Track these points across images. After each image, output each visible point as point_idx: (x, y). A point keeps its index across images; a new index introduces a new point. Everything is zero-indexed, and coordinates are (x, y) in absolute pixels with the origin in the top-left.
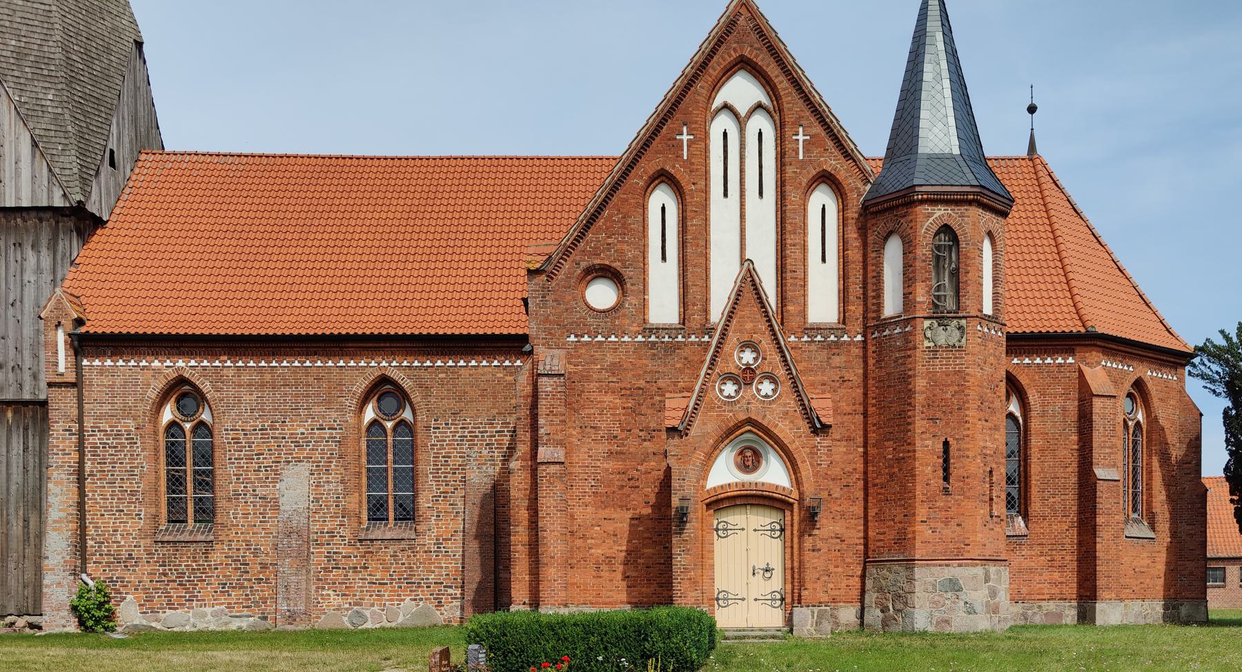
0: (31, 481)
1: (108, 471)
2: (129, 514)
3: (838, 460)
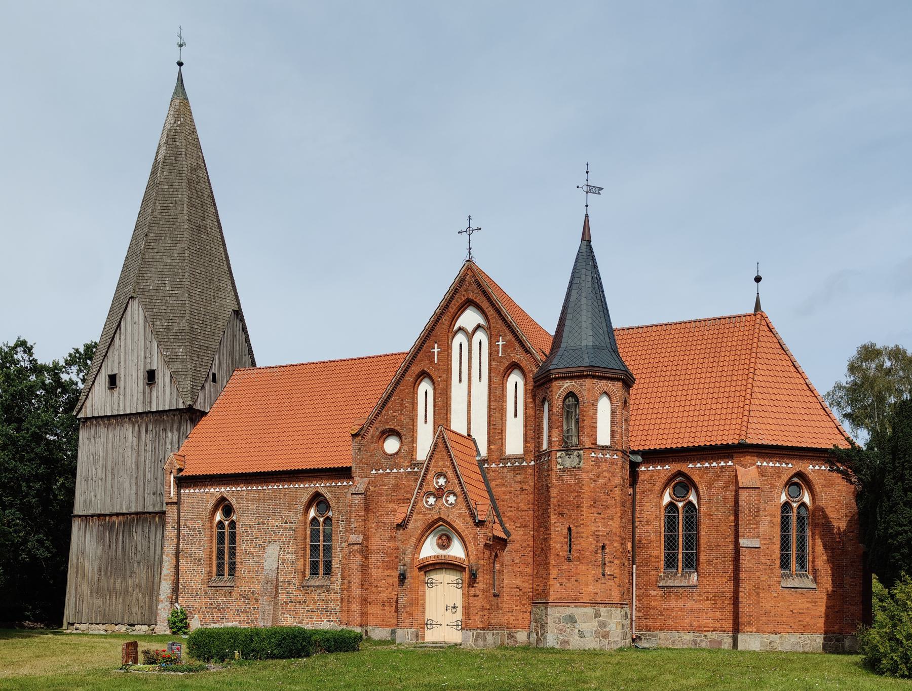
3: (518, 539)
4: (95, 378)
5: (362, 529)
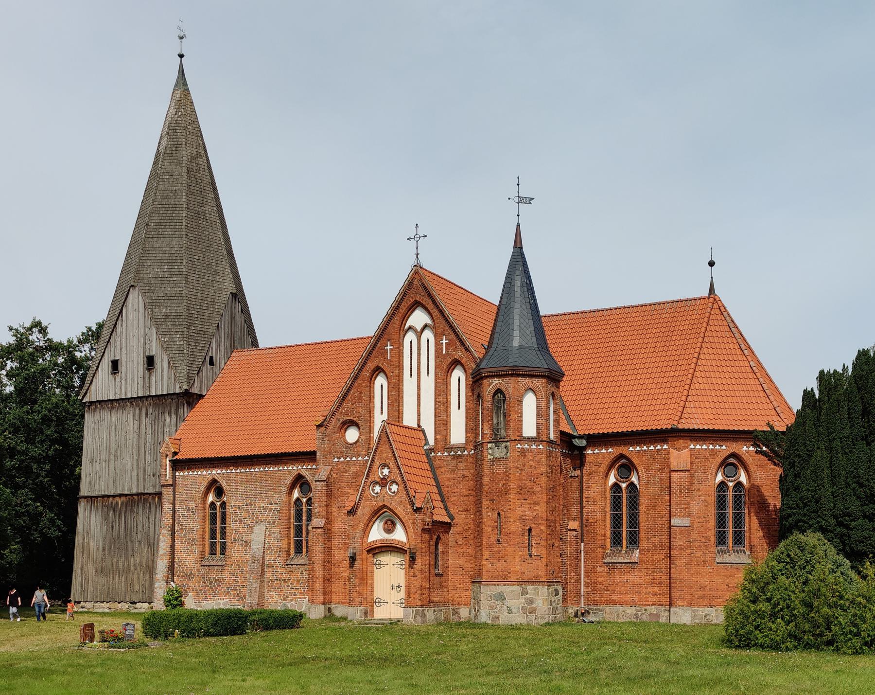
4: (99, 363)
5: (324, 513)
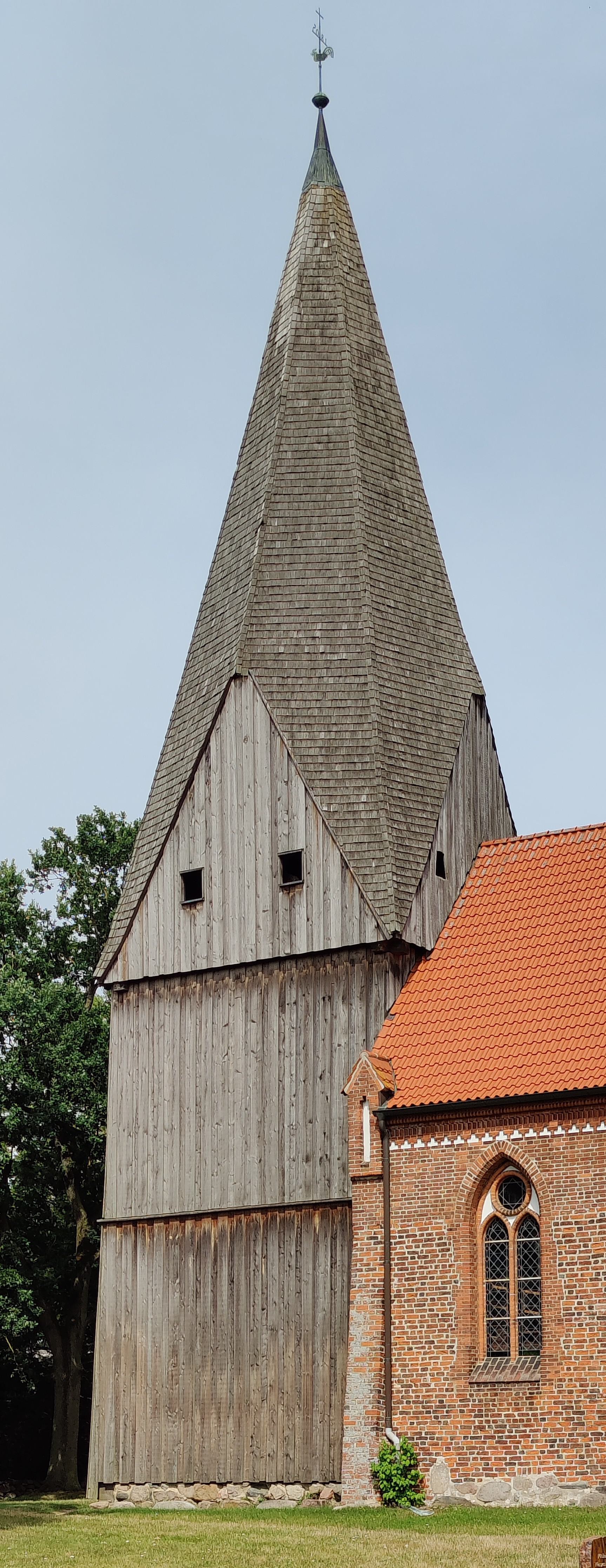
0: (338, 1305)
1: (418, 1289)
2: (439, 1347)
4: (148, 881)
